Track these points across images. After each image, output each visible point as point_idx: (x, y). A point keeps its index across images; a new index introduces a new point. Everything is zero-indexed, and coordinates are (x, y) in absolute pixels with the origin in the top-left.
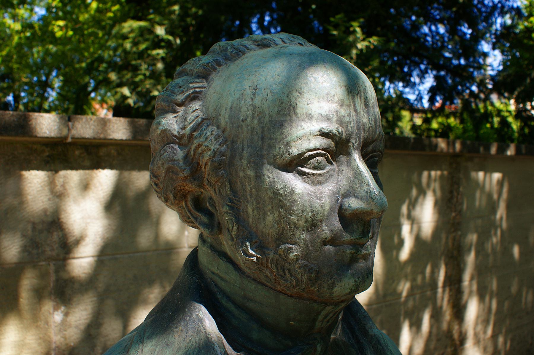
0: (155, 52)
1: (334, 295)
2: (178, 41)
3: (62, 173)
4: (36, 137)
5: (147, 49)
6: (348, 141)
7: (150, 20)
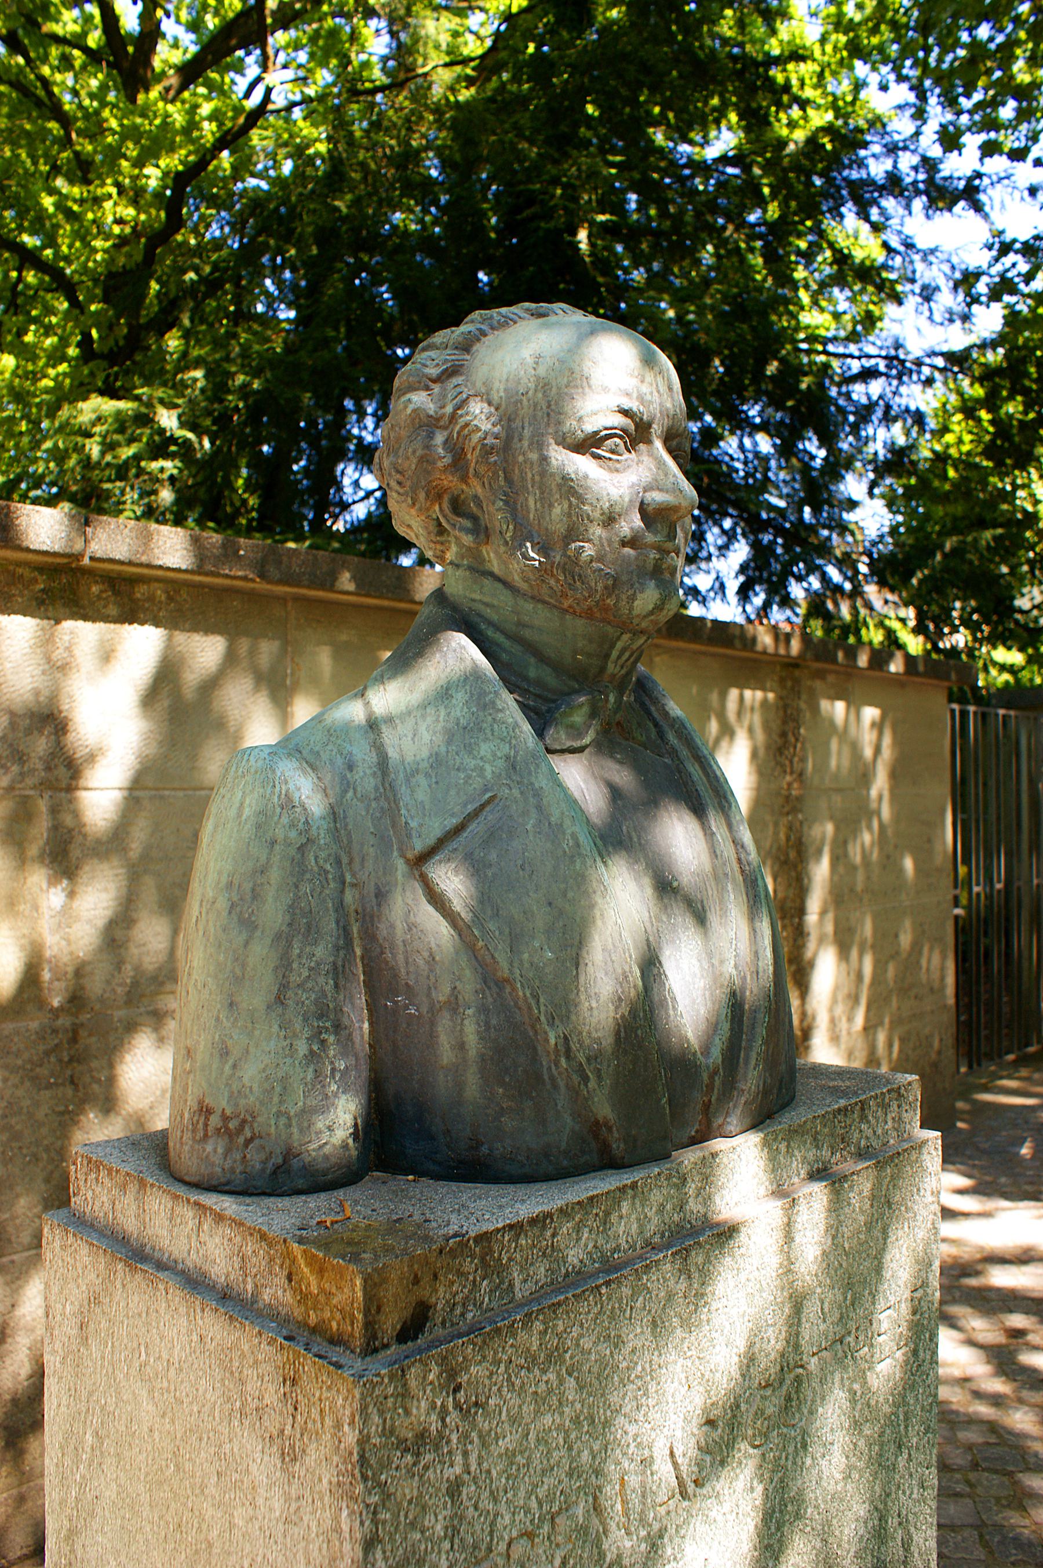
0: (155, 465)
1: (635, 613)
2: (207, 444)
3: (68, 624)
4: (28, 550)
5: (137, 458)
6: (649, 425)
7: (137, 398)
